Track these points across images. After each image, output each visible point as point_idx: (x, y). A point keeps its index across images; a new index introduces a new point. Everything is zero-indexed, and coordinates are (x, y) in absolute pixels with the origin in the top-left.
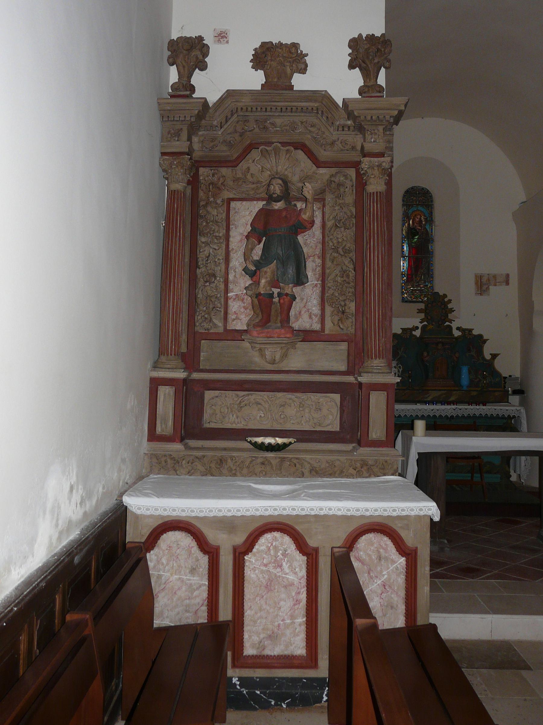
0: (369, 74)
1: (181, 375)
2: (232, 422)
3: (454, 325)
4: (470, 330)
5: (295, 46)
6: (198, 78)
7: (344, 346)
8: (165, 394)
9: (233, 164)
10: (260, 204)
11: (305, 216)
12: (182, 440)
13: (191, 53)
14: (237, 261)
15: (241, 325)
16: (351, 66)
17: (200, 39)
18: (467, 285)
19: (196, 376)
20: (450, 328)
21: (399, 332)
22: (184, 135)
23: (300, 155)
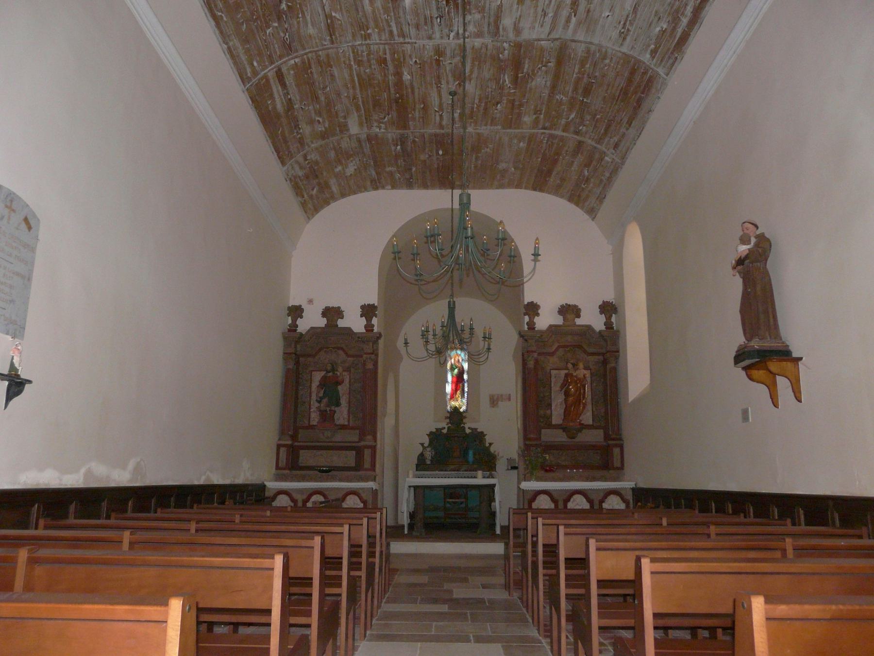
0: (369, 320)
1: (290, 442)
2: (311, 462)
3: (467, 426)
4: (476, 429)
5: (339, 308)
6: (299, 321)
7: (358, 431)
8: (283, 450)
9: (314, 356)
10: (323, 373)
11: (340, 378)
12: (290, 469)
13: (296, 312)
14: (314, 397)
15: (315, 423)
16: (361, 316)
17: (300, 306)
18: (513, 397)
19: (296, 444)
20: (464, 428)
21: (434, 430)
22: (293, 346)
23: (341, 352)
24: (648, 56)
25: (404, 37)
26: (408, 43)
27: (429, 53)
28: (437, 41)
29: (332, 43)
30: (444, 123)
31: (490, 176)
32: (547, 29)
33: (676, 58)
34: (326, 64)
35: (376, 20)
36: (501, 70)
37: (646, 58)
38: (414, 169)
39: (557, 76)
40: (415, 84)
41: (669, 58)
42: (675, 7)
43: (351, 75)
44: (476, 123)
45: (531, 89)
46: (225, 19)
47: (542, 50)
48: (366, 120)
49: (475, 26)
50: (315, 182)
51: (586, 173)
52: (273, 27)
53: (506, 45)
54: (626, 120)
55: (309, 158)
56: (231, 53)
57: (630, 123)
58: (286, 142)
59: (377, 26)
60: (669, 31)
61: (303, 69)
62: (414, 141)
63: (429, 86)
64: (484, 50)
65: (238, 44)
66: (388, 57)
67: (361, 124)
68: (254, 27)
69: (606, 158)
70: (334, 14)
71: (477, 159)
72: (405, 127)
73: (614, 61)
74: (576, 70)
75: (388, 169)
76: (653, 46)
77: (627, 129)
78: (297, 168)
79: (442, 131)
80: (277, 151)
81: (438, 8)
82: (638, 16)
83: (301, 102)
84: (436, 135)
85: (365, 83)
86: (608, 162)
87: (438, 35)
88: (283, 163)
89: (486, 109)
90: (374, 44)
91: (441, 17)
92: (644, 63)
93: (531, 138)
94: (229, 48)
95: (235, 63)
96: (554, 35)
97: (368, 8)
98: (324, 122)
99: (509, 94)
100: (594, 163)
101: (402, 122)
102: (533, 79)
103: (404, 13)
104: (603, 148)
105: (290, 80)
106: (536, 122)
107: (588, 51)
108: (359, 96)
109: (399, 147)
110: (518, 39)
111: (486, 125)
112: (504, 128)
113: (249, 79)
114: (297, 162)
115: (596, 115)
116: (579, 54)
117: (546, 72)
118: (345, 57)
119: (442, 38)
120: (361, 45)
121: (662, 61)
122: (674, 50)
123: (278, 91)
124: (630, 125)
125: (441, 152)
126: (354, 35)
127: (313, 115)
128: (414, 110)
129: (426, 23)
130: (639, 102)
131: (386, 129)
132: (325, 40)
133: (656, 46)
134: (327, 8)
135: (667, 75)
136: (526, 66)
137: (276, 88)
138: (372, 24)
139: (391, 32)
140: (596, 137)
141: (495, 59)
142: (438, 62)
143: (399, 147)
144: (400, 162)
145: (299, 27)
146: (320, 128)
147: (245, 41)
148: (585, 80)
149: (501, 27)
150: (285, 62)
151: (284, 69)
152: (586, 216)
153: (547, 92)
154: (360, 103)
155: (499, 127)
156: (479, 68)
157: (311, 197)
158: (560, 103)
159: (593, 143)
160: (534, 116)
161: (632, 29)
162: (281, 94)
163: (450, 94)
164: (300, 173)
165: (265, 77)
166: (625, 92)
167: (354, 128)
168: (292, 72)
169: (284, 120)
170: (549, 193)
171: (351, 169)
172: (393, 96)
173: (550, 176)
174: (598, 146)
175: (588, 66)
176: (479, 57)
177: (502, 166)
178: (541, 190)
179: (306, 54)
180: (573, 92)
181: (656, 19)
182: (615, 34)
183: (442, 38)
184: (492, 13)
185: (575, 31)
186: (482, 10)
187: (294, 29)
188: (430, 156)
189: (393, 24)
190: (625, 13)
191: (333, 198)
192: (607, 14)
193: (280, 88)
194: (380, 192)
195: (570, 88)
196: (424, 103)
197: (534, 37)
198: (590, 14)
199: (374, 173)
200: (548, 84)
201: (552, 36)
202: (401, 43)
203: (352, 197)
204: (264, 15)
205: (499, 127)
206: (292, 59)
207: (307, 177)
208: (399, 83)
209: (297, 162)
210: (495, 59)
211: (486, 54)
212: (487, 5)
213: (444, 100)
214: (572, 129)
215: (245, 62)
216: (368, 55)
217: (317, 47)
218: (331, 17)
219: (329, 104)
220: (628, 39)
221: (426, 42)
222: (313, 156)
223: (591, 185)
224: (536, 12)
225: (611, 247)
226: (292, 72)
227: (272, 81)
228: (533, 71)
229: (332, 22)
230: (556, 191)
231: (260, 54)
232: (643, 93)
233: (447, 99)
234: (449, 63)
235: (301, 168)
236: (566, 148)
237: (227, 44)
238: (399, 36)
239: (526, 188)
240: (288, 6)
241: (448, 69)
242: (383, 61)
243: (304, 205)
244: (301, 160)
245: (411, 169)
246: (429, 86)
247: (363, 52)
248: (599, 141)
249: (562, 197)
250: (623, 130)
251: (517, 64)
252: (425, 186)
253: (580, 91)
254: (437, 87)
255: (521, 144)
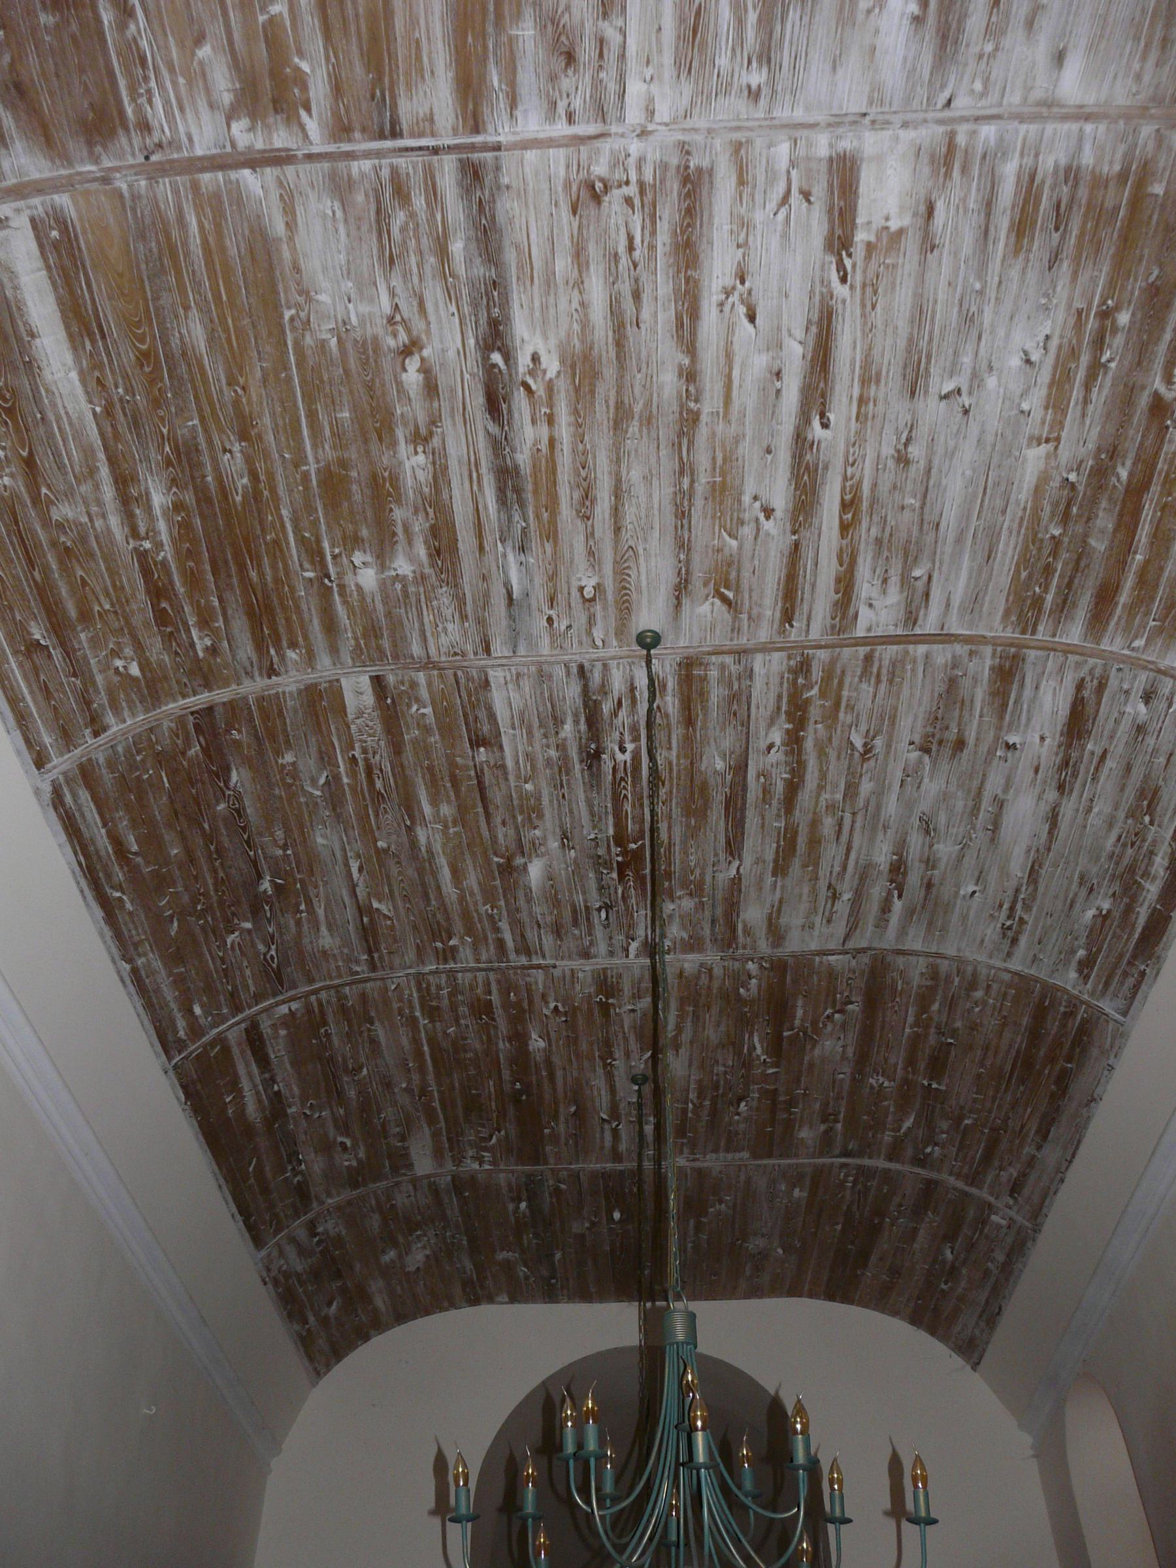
24: (1073, 975)
25: (528, 953)
26: (538, 967)
27: (584, 988)
28: (601, 961)
29: (373, 967)
30: (623, 1147)
31: (727, 1270)
32: (840, 928)
33: (1143, 974)
34: (359, 1015)
35: (466, 915)
36: (744, 1023)
37: (1069, 979)
38: (558, 1256)
39: (867, 1036)
40: (556, 1059)
41: (1126, 974)
42: (1126, 861)
43: (416, 1041)
44: (693, 1146)
45: (811, 1065)
46: (129, 906)
47: (832, 975)
48: (450, 1144)
49: (683, 927)
50: (336, 1285)
51: (949, 1255)
52: (243, 931)
53: (751, 966)
54: (1033, 1127)
55: (320, 1229)
56: (139, 982)
57: (1044, 1134)
58: (265, 1191)
59: (470, 930)
60: (1116, 914)
61: (307, 1028)
62: (557, 1192)
63: (586, 1064)
64: (704, 979)
65: (158, 964)
66: (495, 997)
67: (438, 1154)
68: (197, 930)
69: (994, 1218)
70: (376, 905)
71: (698, 1228)
72: (537, 1157)
73: (994, 993)
74: (910, 1019)
75: (501, 1256)
76: (1081, 953)
77: (1039, 1148)
78: (291, 1251)
79: (620, 1167)
80: (244, 1210)
81: (601, 888)
82: (1041, 889)
83: (304, 1098)
84: (605, 1175)
85: (447, 1057)
86: (999, 1227)
87: (602, 948)
88: (258, 1241)
89: (714, 1112)
90: (465, 970)
91: (608, 907)
92: (1065, 991)
93: (819, 1176)
94: (135, 971)
95: (149, 1006)
96: (859, 941)
97: (449, 890)
98: (355, 1145)
99: (765, 1078)
100: (966, 1230)
101: (530, 1145)
102: (815, 1043)
103: (529, 900)
104: (985, 1195)
105: (278, 1050)
106: (826, 1143)
107: (934, 974)
108: (433, 1087)
109: (523, 1205)
110: (779, 952)
111: (715, 1150)
112: (755, 1156)
113: (181, 1045)
114: (293, 1240)
115: (961, 1118)
116: (915, 983)
117: (844, 1026)
118: (401, 1000)
119: (611, 954)
120: (435, 972)
121: (1107, 984)
122: (1134, 956)
123: (250, 1075)
124: (1045, 1137)
125: (617, 1215)
126: (420, 951)
127: (332, 1132)
128: (555, 1117)
129: (575, 923)
130: (1063, 1081)
131: (494, 1163)
132: (357, 962)
133: (1089, 950)
134: (361, 892)
135: (1125, 1014)
136: (800, 1013)
137: (246, 1070)
138: (458, 926)
139: (501, 943)
140: (965, 1170)
141: (731, 999)
142: (605, 1008)
143: (523, 1205)
144: (528, 1238)
145: (299, 934)
146: (347, 1161)
147: (175, 956)
148: (932, 1040)
149: (740, 927)
150: (266, 1010)
151: (265, 1026)
152: (957, 1361)
153: (847, 1069)
154: (436, 1104)
155: (745, 1155)
156: (696, 1018)
157: (324, 1321)
158: (880, 1092)
159: (960, 1184)
160: (823, 1127)
161: (1030, 919)
162: (258, 1080)
163: (634, 1080)
164: (299, 1266)
165: (220, 1040)
166: (1026, 1063)
167: (423, 1164)
168: (283, 1032)
169: (263, 1142)
170: (865, 1306)
171: (417, 1257)
172: (507, 1087)
173: (865, 1266)
174: (973, 1190)
175: (935, 1007)
176: (694, 995)
177: (755, 1244)
178: (847, 1299)
179: (315, 992)
180: (905, 1069)
181: (1083, 893)
182: (991, 932)
183: (611, 954)
184: (720, 896)
185: (903, 932)
186: (697, 890)
187: (287, 937)
188: (593, 1224)
189: (504, 925)
190: (1011, 885)
191: (378, 1325)
192: (971, 889)
193: (254, 1067)
194: (485, 1309)
195: (898, 1059)
196: (576, 1102)
197: (813, 946)
198: (934, 890)
199: (469, 1265)
200: (850, 1051)
201: (850, 945)
202: (524, 967)
203: (420, 1322)
204: (221, 903)
205: (745, 1155)
206: (283, 1002)
207: (315, 1274)
208: (521, 1057)
209: (293, 1240)
210: (731, 999)
211: (709, 988)
212: (708, 879)
213: (621, 1094)
214: (909, 1152)
215: (173, 1005)
216: (451, 995)
217: (340, 976)
218: (370, 911)
219: (367, 1106)
220: (1023, 941)
221: (576, 964)
222: (330, 1225)
223: (963, 1284)
224: (814, 892)
225: (1027, 1439)
226: (283, 1032)
227: (236, 1051)
228: (814, 1023)
229: (371, 920)
230: (881, 1301)
231: (210, 989)
232: (1069, 1059)
233: (628, 1093)
234: (630, 1010)
235: (302, 1252)
236: (896, 1200)
237: (130, 961)
238: (517, 952)
239: (811, 1296)
240: (277, 887)
241: (627, 1021)
242: (482, 1009)
243: (306, 1342)
244: (302, 1234)
245: (553, 1255)
246: (586, 1064)
247: (439, 988)
248: (974, 1179)
249: (894, 1313)
250: (1028, 1150)
251: (778, 1007)
252: (585, 1296)
253: (922, 1065)
254: (605, 1065)
255: (797, 1193)
